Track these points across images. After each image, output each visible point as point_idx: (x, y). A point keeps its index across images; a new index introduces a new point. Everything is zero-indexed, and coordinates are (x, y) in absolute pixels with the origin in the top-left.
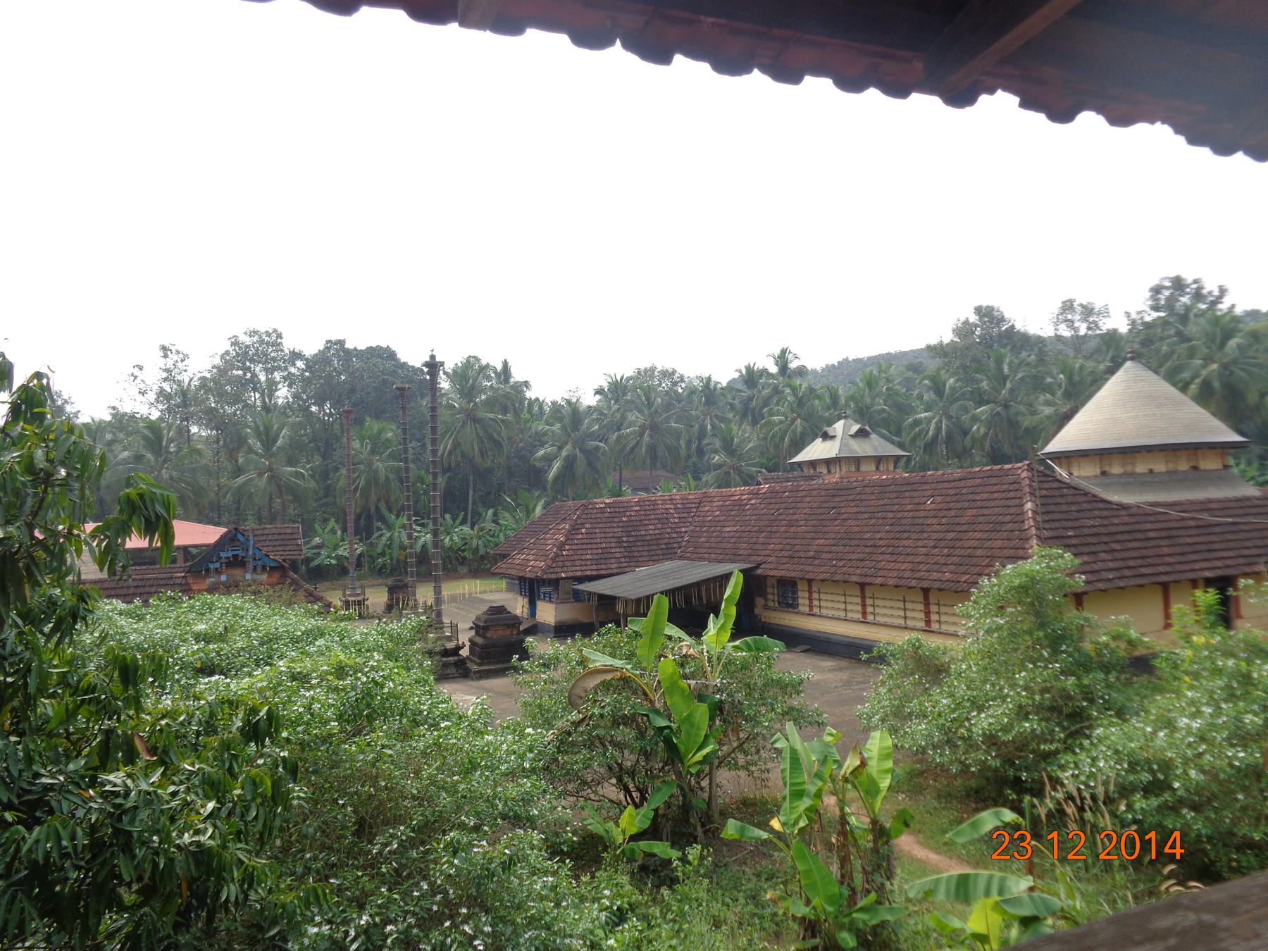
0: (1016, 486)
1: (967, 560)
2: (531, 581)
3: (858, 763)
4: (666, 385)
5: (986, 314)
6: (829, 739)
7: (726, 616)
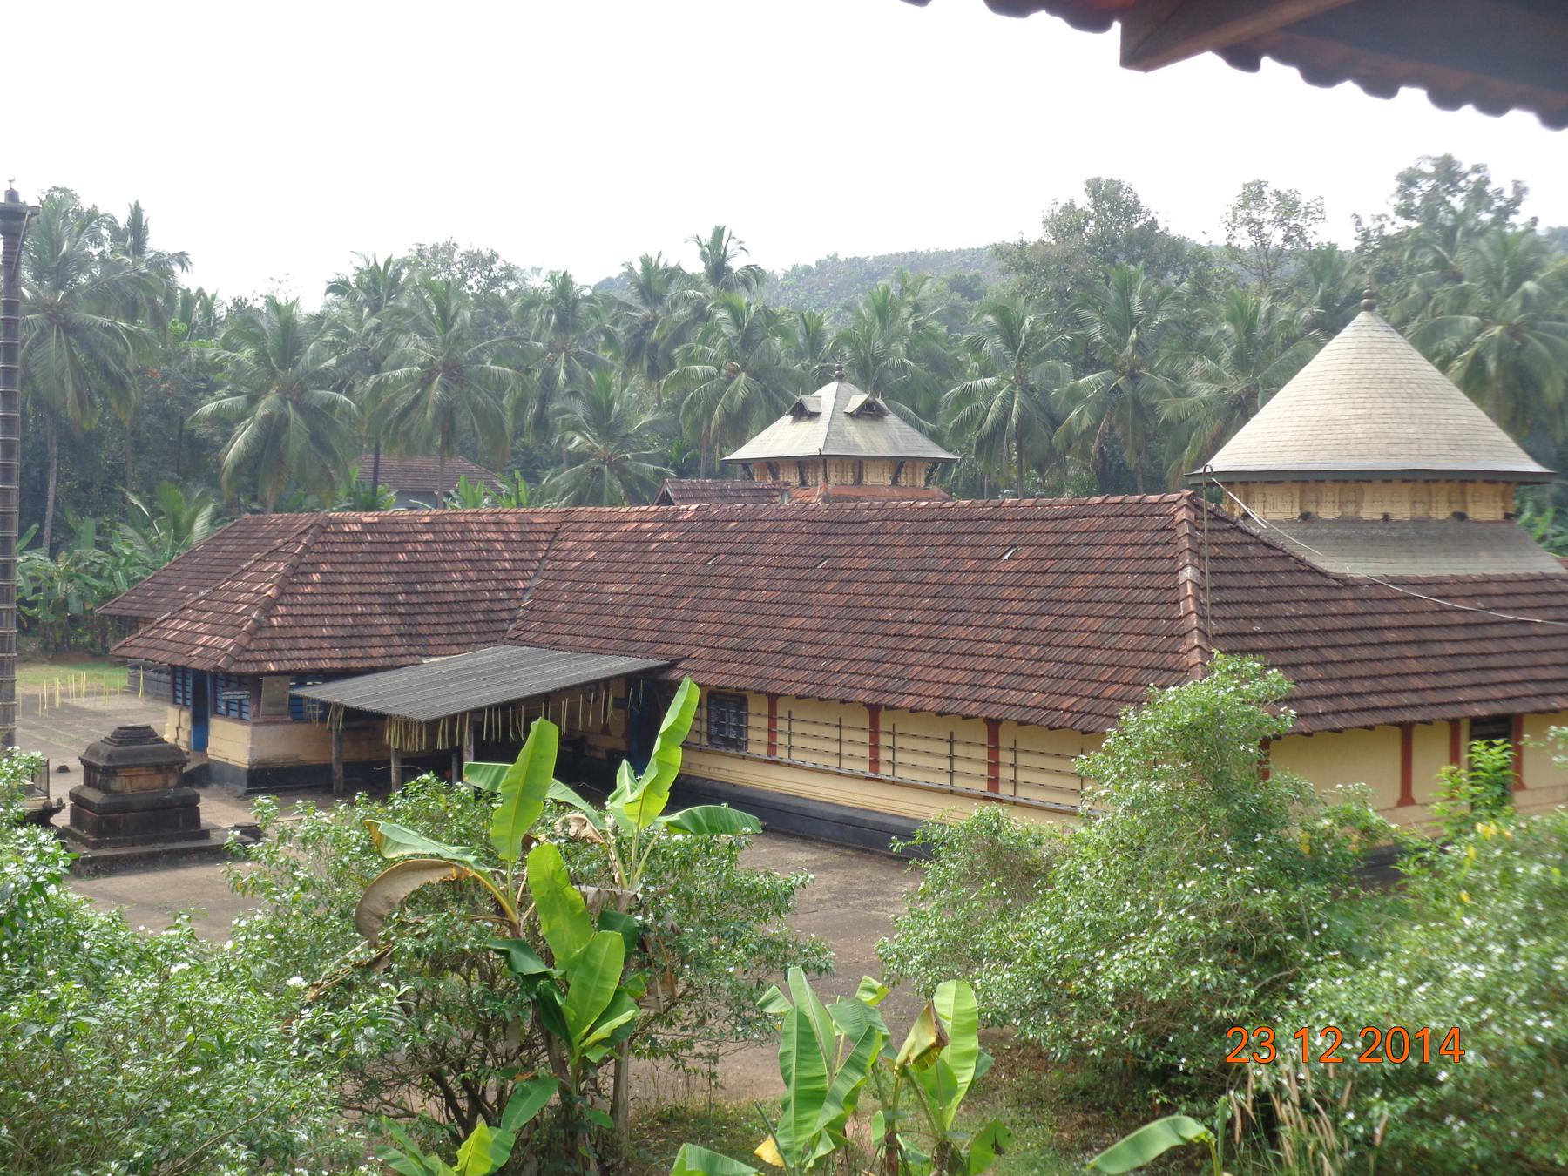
0: (1167, 536)
2: (200, 676)
3: (932, 1040)
4: (475, 283)
5: (1107, 194)
6: (867, 997)
7: (663, 766)
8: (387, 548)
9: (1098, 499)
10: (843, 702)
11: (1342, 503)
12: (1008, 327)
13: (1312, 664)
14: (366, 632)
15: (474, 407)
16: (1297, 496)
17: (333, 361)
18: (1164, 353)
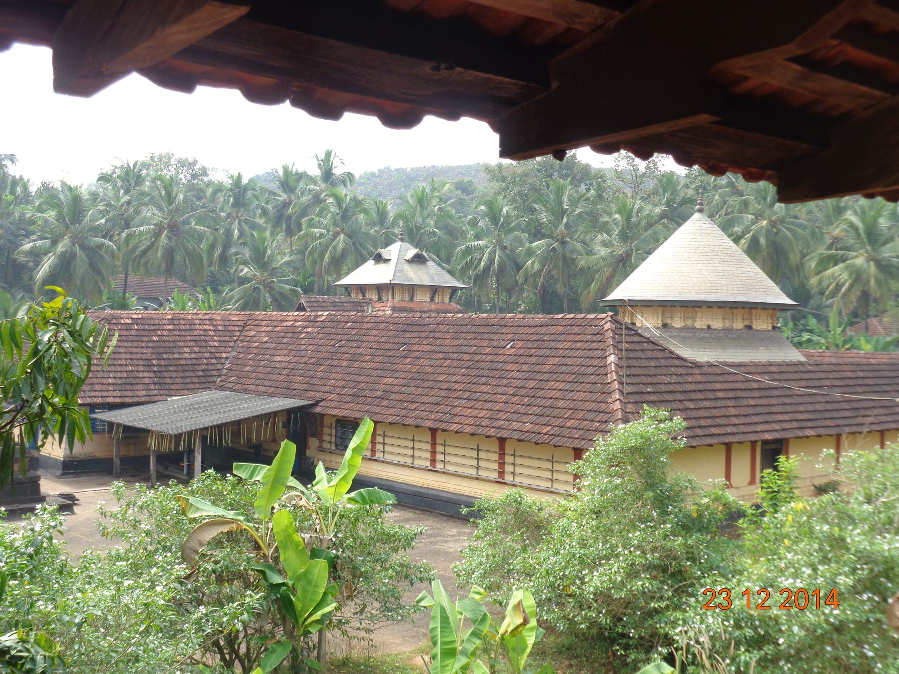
1: (550, 411)
4: (184, 177)
8: (146, 333)
9: (572, 316)
10: (417, 427)
11: (686, 318)
12: (494, 215)
13: (679, 410)
14: (134, 381)
15: (186, 249)
16: (660, 314)
17: (103, 221)
18: (581, 229)
